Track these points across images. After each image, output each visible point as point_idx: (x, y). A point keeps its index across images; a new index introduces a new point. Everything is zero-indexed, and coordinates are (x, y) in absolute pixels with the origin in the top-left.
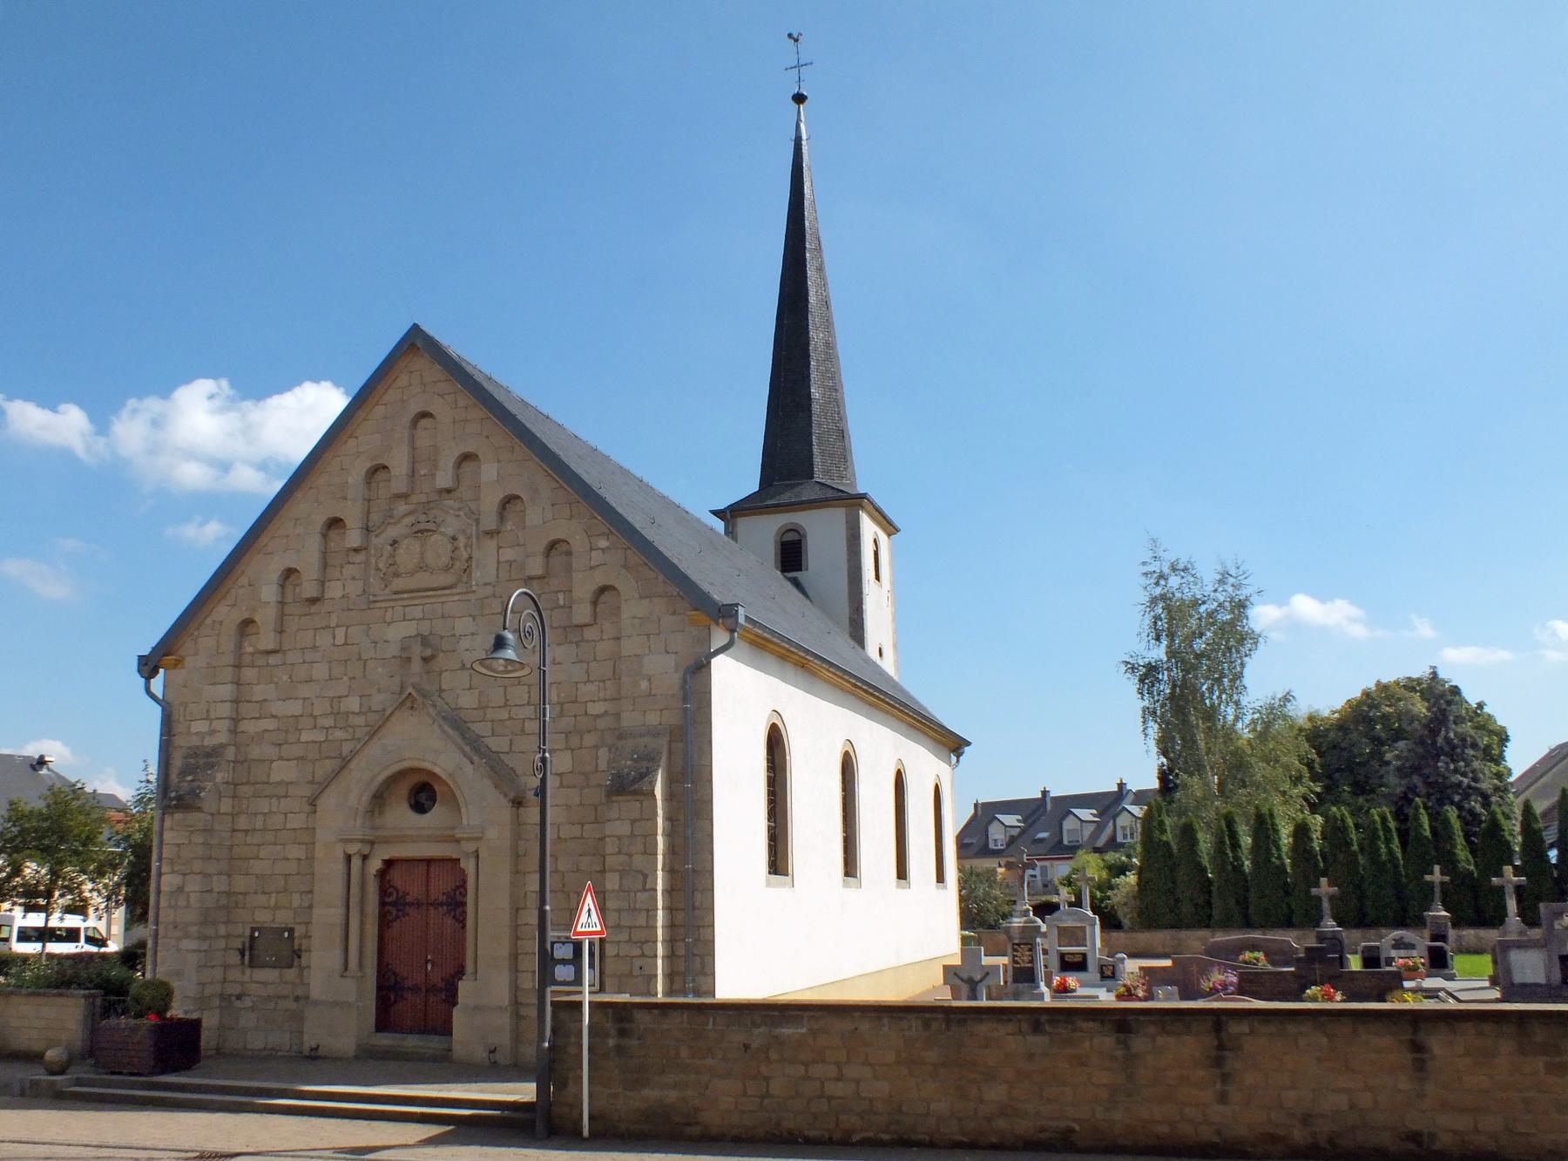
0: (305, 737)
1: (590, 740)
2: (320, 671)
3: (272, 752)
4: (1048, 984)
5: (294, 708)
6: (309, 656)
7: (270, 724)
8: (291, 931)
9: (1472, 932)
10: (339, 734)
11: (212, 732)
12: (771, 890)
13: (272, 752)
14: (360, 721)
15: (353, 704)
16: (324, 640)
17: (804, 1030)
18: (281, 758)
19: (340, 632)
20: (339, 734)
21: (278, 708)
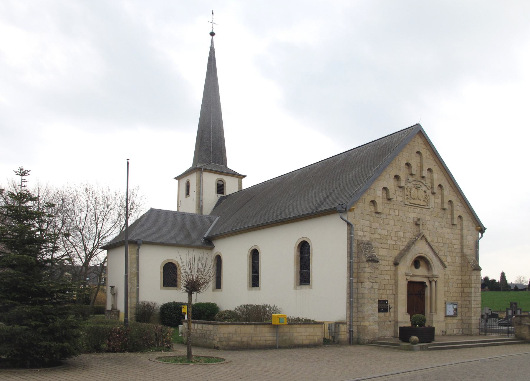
0: (389, 242)
1: (454, 254)
2: (392, 222)
3: (379, 245)
4: (41, 341)
5: (384, 232)
6: (388, 217)
7: (379, 237)
8: (387, 301)
9: (200, 326)
10: (399, 243)
11: (365, 236)
12: (251, 291)
13: (379, 245)
14: (404, 240)
15: (401, 234)
16: (392, 212)
17: (19, 353)
18: (382, 248)
19: (397, 211)
20: (399, 243)
21: (379, 231)
